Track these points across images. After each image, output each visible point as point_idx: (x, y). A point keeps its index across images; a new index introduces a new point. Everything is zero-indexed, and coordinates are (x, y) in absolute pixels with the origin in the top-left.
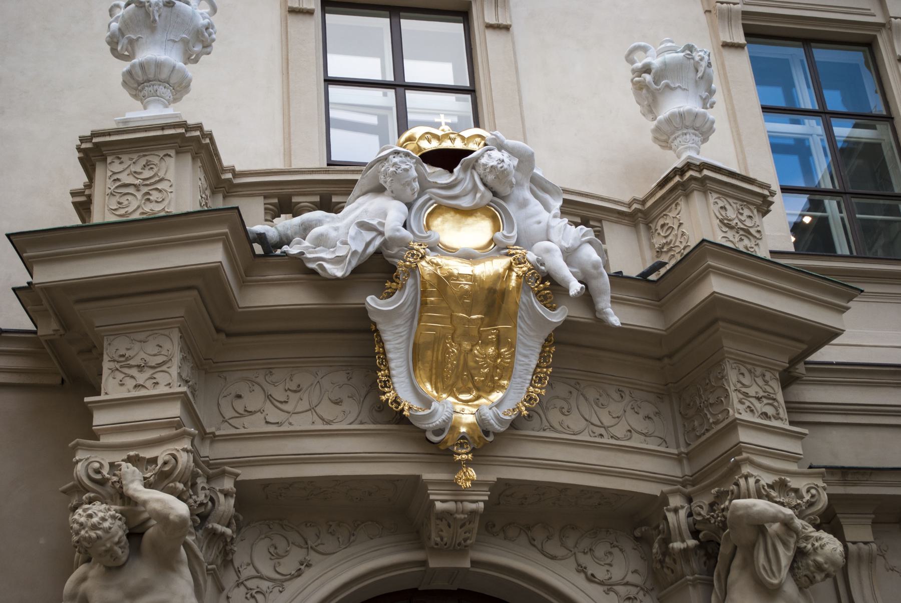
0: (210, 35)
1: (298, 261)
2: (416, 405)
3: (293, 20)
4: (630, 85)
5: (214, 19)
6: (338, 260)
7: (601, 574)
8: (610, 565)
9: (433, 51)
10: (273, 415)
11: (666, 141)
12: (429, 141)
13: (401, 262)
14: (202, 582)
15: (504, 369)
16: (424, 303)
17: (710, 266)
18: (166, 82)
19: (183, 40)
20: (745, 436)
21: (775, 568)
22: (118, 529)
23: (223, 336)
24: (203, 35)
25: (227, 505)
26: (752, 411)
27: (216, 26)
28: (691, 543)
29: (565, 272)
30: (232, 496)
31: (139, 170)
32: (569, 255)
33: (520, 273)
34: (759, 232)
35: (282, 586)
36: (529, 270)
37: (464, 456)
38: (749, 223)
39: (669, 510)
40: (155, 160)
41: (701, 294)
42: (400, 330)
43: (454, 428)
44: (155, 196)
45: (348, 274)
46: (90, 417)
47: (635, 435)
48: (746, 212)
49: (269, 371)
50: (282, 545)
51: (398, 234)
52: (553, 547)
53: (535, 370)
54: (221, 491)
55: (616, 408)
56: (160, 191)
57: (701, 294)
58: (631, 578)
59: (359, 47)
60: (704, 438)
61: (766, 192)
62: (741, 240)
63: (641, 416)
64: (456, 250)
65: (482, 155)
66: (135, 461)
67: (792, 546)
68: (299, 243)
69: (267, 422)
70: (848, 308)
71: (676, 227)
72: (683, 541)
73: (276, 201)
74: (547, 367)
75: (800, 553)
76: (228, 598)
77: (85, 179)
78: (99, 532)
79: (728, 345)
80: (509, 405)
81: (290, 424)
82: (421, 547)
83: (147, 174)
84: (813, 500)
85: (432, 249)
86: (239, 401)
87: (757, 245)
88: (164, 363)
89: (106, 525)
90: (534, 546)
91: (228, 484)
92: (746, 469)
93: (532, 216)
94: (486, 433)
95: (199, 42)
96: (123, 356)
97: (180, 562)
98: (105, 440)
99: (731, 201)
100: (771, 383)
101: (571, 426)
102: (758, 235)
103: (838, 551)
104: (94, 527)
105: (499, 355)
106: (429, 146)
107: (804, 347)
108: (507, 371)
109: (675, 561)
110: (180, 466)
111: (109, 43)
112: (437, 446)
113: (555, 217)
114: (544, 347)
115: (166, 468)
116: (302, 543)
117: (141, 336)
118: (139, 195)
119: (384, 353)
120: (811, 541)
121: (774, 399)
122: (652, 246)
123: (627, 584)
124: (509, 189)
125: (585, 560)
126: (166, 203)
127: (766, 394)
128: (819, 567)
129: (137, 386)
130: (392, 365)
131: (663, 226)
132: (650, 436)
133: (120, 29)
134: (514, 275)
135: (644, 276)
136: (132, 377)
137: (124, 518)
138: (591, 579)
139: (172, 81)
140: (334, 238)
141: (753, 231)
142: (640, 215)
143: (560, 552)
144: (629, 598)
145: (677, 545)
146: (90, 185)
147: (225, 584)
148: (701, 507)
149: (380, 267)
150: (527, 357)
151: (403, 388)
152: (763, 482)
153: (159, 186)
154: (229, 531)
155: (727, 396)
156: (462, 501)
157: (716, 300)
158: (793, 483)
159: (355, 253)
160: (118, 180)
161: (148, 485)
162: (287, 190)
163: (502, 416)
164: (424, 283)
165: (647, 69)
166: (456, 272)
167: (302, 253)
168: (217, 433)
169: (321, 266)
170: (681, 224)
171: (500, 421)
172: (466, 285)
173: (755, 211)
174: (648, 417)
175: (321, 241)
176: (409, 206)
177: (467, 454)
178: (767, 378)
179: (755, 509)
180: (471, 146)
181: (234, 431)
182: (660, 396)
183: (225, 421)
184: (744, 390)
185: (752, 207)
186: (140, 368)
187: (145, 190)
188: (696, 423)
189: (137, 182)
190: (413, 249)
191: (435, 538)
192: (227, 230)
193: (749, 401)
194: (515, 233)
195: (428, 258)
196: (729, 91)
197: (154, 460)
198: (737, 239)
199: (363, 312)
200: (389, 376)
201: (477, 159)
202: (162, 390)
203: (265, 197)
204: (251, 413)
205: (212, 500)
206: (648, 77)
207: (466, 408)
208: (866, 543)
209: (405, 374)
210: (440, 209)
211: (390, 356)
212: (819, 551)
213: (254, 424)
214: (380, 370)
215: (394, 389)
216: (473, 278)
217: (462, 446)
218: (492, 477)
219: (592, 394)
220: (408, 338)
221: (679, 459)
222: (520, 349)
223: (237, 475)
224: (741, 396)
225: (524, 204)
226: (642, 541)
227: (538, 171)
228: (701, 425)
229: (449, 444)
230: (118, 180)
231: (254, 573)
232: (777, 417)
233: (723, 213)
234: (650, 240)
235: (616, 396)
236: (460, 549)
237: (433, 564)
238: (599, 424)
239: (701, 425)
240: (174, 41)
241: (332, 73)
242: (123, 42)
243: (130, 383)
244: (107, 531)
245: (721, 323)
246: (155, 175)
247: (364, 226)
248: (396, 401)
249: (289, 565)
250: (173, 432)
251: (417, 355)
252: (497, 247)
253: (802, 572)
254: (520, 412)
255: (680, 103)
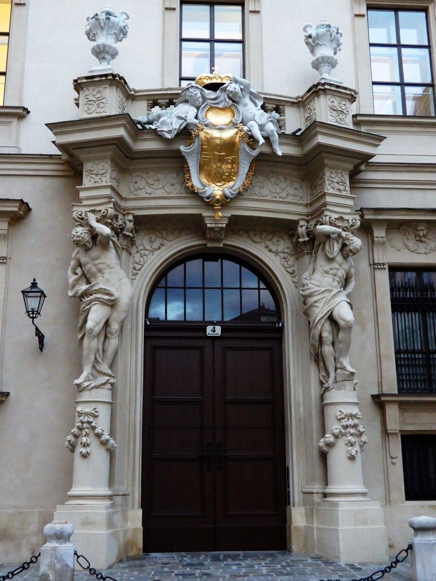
0: (126, 30)
1: (155, 131)
2: (200, 186)
3: (168, 13)
4: (304, 43)
5: (128, 22)
6: (170, 132)
7: (274, 248)
8: (278, 245)
9: (228, 22)
10: (149, 190)
11: (317, 68)
12: (207, 80)
13: (193, 132)
14: (120, 254)
15: (235, 173)
16: (202, 148)
17: (317, 131)
18: (108, 53)
19: (115, 34)
20: (328, 199)
21: (332, 251)
22: (87, 237)
23: (129, 160)
24: (123, 30)
25: (130, 225)
26: (334, 188)
27: (129, 26)
28: (307, 239)
29: (258, 134)
30: (132, 222)
31: (95, 94)
32: (261, 127)
33: (240, 136)
34: (348, 111)
35: (153, 253)
36: (244, 134)
37: (218, 207)
38: (344, 107)
39: (299, 226)
40: (101, 89)
41: (314, 143)
42: (194, 158)
43: (214, 197)
44: (101, 105)
45: (173, 137)
46: (79, 194)
47: (290, 196)
48: (343, 102)
49: (148, 173)
50: (154, 237)
51: (191, 121)
52: (257, 239)
53: (247, 173)
54: (128, 220)
55: (283, 185)
56: (103, 103)
57: (314, 143)
58: (286, 250)
59: (196, 23)
60: (316, 198)
61: (353, 93)
62: (339, 115)
63: (293, 188)
64: (216, 126)
65: (228, 86)
66: (93, 211)
67: (340, 243)
68: (156, 124)
69: (146, 193)
70: (379, 145)
71: (313, 110)
72: (304, 238)
73: (151, 102)
74: (252, 172)
75: (344, 245)
76: (133, 257)
77: (78, 95)
78: (80, 238)
79: (326, 161)
80: (236, 187)
81: (155, 194)
82: (205, 239)
83: (98, 95)
84: (354, 224)
85: (206, 126)
86: (136, 184)
87: (346, 117)
88: (103, 174)
89: (82, 236)
90: (249, 238)
91: (131, 217)
92: (326, 213)
93: (249, 110)
94: (227, 198)
95: (122, 33)
96: (90, 170)
97: (110, 248)
98: (85, 203)
99: (337, 98)
100: (345, 176)
101: (263, 193)
102: (346, 113)
103: (359, 245)
104: (78, 237)
105: (233, 168)
106: (207, 82)
107: (360, 161)
108: (236, 174)
109: (301, 245)
110: (109, 214)
111: (86, 35)
112: (209, 203)
113: (258, 110)
114: (251, 164)
115: (104, 214)
116: (161, 237)
117: (97, 162)
118: (95, 104)
119: (188, 167)
120: (349, 241)
121: (345, 183)
122: (305, 116)
123: (284, 253)
124: (239, 99)
125: (268, 243)
126: (105, 108)
127: (341, 181)
128: (351, 251)
129: (95, 182)
130: (191, 172)
131: (309, 108)
132: (296, 196)
133: (90, 29)
134: (238, 136)
135: (294, 134)
136: (94, 178)
137: (90, 233)
138: (270, 251)
139: (110, 52)
140: (170, 120)
141: (345, 111)
142: (301, 103)
143: (258, 240)
144: (284, 258)
145: (301, 240)
146: (79, 97)
147: (131, 252)
148: (311, 225)
149: (186, 133)
150: (244, 168)
151: (197, 180)
152: (333, 218)
153: (102, 101)
154: (131, 235)
155: (324, 182)
156: (217, 224)
157: (320, 146)
158: (346, 217)
159: (175, 129)
160: (87, 98)
161: (98, 221)
162: (156, 98)
163: (232, 192)
164: (202, 141)
165: (310, 37)
166: (214, 136)
167: (156, 129)
168: (128, 197)
169: (163, 134)
170: (315, 109)
171: (232, 194)
172: (218, 142)
173: (348, 102)
174: (296, 189)
175: (163, 123)
176: (198, 108)
177: (219, 206)
178: (343, 174)
179: (325, 230)
180: (224, 81)
181: (134, 197)
182: (302, 180)
183: (131, 192)
184: (332, 180)
185: (346, 100)
186: (96, 175)
187: (97, 102)
188: (314, 191)
189: (94, 99)
190: (198, 127)
191: (208, 236)
192: (125, 122)
193: (335, 183)
194: (241, 118)
195: (204, 130)
196: (355, 38)
197: (100, 211)
198: (337, 115)
199: (179, 151)
200: (190, 176)
201: (226, 87)
202: (104, 184)
203: (148, 100)
204: (141, 189)
205: (124, 223)
206: (310, 40)
207: (219, 188)
208: (382, 237)
209: (196, 175)
210: (211, 108)
211: (190, 168)
212: (351, 244)
213: (142, 194)
214: (186, 174)
215: (192, 181)
216: (221, 139)
217: (217, 203)
218: (229, 215)
219: (273, 180)
220: (197, 162)
221: (306, 205)
222: (241, 165)
223: (134, 214)
224: (330, 182)
225: (245, 105)
226: (291, 236)
227: (252, 90)
228: (316, 192)
229: (213, 202)
230: (87, 98)
231: (143, 248)
232: (345, 190)
233: (332, 104)
234: (304, 114)
235: (283, 180)
236: (219, 240)
237: (209, 245)
238: (275, 192)
239: (316, 192)
240: (110, 34)
241: (184, 36)
242: (91, 35)
243: (93, 181)
244: (83, 238)
245: (323, 154)
246: (101, 96)
247: (180, 118)
248: (192, 186)
249: (156, 245)
250: (107, 200)
251: (201, 168)
252: (234, 125)
253: (345, 252)
254: (240, 190)
255: (325, 51)
